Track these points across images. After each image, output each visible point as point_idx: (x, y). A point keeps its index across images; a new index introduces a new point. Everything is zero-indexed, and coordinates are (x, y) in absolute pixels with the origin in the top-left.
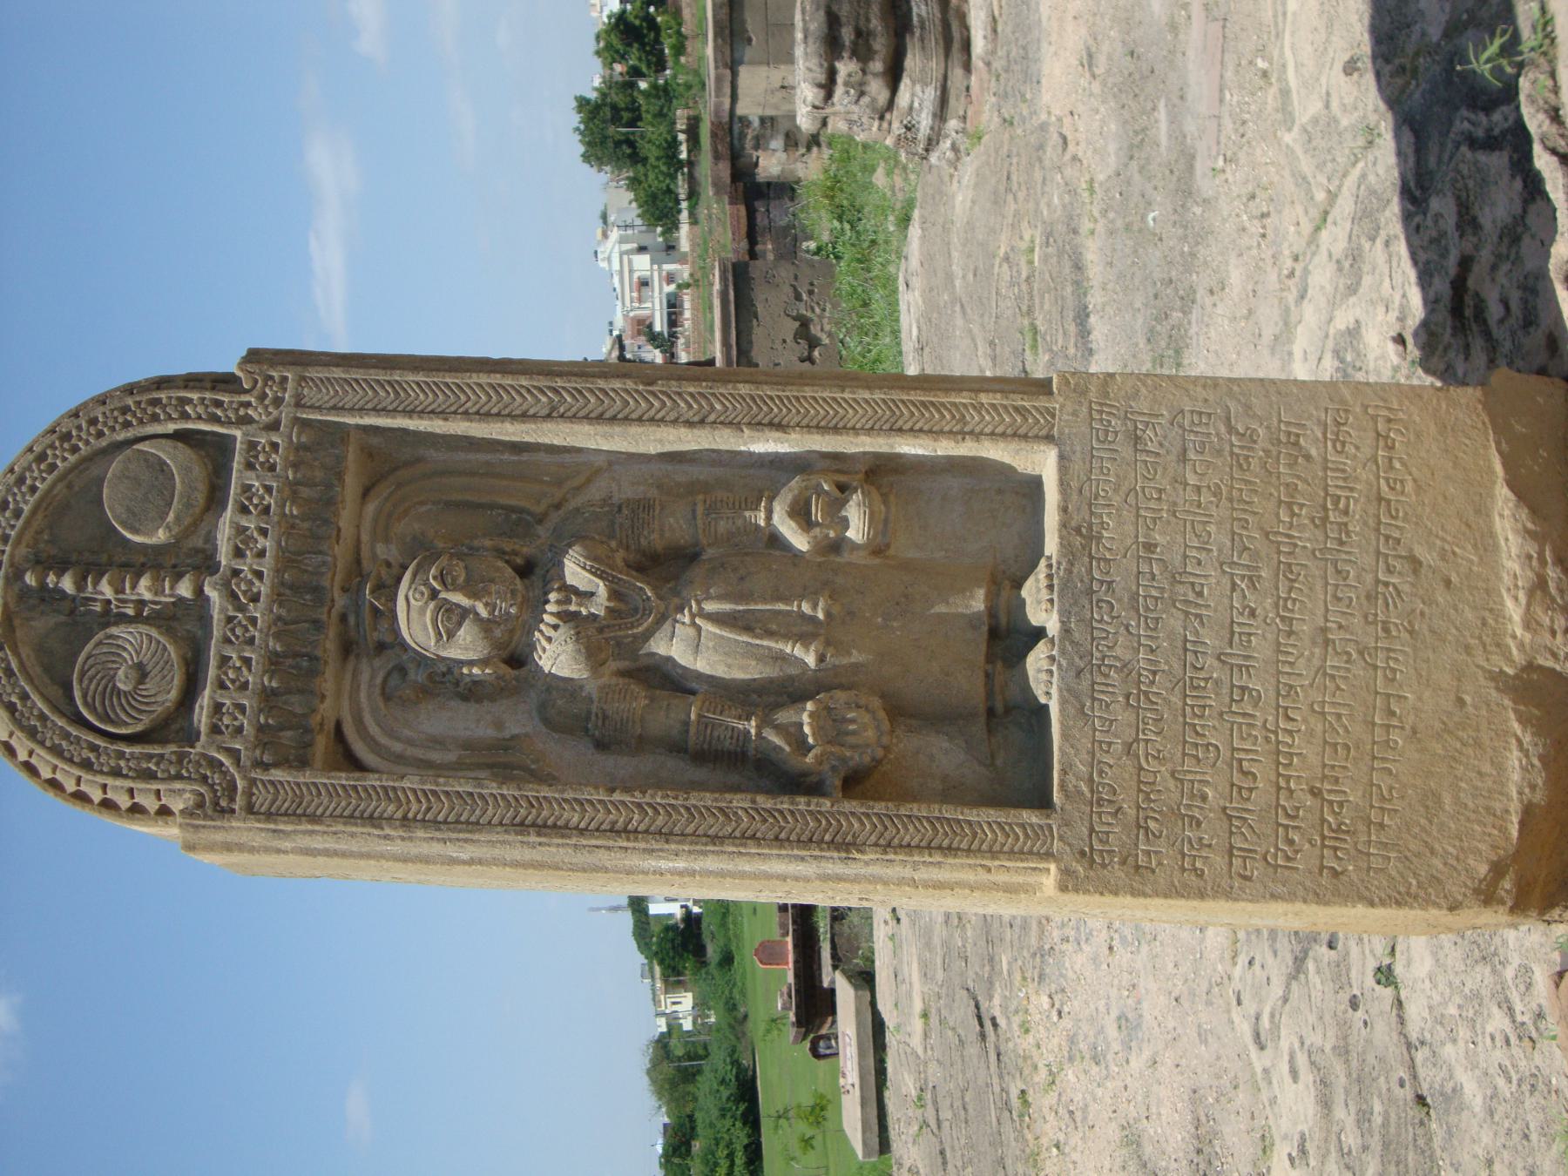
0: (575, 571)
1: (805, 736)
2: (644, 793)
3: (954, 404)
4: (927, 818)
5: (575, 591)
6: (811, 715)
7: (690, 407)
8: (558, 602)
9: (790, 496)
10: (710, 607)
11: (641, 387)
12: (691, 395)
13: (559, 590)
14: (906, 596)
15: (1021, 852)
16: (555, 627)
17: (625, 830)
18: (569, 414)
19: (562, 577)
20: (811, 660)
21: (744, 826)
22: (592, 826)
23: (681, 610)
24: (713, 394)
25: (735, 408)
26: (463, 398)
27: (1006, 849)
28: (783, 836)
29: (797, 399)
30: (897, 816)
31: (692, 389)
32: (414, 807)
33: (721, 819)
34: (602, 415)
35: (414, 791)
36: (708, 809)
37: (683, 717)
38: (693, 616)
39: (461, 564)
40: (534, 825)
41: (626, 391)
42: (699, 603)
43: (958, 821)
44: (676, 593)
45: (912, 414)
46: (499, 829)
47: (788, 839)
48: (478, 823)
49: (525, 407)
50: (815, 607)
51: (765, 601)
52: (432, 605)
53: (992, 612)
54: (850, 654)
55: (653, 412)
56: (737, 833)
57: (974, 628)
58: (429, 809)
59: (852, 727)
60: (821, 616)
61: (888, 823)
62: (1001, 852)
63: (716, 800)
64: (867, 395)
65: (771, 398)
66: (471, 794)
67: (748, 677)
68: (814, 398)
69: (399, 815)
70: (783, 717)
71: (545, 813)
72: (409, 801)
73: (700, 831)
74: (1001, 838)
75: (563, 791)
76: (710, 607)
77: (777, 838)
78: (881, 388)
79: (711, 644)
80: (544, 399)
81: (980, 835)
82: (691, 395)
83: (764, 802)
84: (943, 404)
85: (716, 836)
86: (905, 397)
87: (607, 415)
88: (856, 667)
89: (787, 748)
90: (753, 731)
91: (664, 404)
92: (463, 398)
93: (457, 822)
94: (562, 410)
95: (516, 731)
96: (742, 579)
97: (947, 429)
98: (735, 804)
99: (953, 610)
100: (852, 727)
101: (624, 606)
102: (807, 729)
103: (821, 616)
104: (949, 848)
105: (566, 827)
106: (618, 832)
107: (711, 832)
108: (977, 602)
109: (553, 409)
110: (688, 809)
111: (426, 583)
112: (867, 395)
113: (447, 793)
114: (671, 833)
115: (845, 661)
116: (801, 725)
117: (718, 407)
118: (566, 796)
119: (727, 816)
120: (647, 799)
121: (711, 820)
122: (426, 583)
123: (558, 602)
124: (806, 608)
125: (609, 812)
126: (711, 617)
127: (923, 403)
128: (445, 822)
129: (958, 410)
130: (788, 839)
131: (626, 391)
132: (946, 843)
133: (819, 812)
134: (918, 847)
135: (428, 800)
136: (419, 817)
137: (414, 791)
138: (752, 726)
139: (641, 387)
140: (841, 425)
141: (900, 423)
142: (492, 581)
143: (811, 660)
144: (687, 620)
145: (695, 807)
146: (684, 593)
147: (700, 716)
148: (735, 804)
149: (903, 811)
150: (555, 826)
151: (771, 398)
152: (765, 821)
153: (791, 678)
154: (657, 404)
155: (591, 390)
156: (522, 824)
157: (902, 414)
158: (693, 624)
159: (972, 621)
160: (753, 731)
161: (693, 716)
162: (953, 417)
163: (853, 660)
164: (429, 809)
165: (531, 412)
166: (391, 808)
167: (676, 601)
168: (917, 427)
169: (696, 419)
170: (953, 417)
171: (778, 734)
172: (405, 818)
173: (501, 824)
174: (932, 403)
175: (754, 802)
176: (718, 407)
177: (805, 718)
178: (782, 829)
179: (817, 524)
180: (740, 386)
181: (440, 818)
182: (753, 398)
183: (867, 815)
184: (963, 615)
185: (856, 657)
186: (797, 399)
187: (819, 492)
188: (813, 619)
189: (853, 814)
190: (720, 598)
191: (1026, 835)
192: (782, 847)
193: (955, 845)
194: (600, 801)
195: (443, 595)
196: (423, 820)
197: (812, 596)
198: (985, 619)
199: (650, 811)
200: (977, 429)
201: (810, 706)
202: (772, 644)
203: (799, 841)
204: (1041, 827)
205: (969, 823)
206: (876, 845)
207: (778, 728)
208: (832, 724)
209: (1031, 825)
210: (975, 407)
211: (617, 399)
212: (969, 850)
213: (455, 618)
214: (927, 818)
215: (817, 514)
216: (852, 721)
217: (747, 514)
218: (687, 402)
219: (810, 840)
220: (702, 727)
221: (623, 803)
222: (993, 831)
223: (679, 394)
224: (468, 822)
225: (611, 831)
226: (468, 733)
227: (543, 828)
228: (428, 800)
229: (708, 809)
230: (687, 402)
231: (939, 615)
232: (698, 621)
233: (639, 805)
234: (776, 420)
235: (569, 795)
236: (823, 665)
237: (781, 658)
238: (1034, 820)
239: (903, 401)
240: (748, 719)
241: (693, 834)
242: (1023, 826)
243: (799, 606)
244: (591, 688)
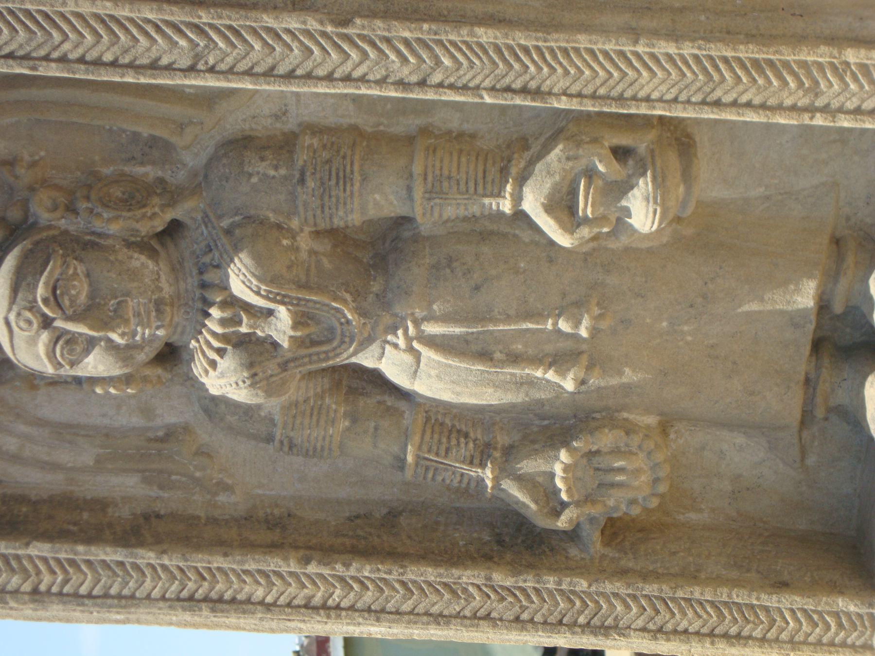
0: (241, 280)
1: (556, 491)
2: (347, 565)
3: (804, 64)
4: (712, 603)
5: (247, 307)
6: (566, 469)
7: (405, 60)
8: (223, 322)
9: (548, 185)
10: (432, 329)
11: (329, 29)
12: (406, 42)
13: (224, 305)
14: (705, 297)
15: (832, 644)
16: (221, 352)
17: (324, 607)
18: (223, 67)
19: (226, 288)
20: (569, 385)
21: (475, 604)
22: (282, 600)
23: (394, 330)
24: (440, 43)
25: (472, 64)
26: (57, 36)
27: (811, 639)
28: (525, 616)
29: (565, 51)
30: (673, 599)
31: (407, 34)
32: (47, 579)
33: (447, 596)
34: (273, 68)
35: (45, 560)
36: (430, 584)
37: (396, 449)
38: (409, 339)
39: (81, 269)
40: (206, 599)
41: (308, 33)
42: (417, 323)
43: (752, 607)
44: (384, 302)
45: (738, 79)
46: (161, 604)
47: (531, 620)
48: (132, 597)
49: (154, 54)
50: (577, 324)
51: (508, 319)
52: (45, 336)
53: (823, 306)
54: (620, 373)
55: (349, 65)
56: (467, 613)
57: (796, 326)
58: (66, 581)
59: (620, 478)
60: (584, 333)
61: (660, 606)
62: (805, 643)
63: (440, 575)
64: (672, 49)
65: (526, 50)
66: (121, 564)
67: (484, 403)
68: (592, 52)
69: (27, 587)
70: (529, 466)
71: (220, 587)
72: (38, 573)
73: (420, 609)
74: (806, 627)
75: (242, 562)
76: (432, 329)
77: (517, 619)
78: (693, 40)
79: (433, 373)
80: (183, 43)
81: (779, 622)
82: (406, 42)
83: (501, 578)
84: (786, 65)
85: (441, 615)
86: (729, 54)
87: (281, 70)
88: (627, 389)
89: (533, 506)
90: (489, 484)
91: (365, 54)
92: (57, 36)
93: (106, 596)
94: (211, 61)
95: (171, 419)
96: (477, 288)
97: (788, 102)
98: (465, 579)
99: (769, 307)
100: (620, 478)
101: (315, 333)
102: (559, 484)
103: (584, 333)
104: (738, 636)
105: (248, 601)
106: (315, 609)
107: (435, 610)
108: (805, 297)
109: (197, 57)
110: (403, 584)
111: (32, 307)
112: (672, 49)
113: (89, 563)
114: (383, 611)
115: (614, 381)
116: (552, 475)
117: (447, 61)
118: (246, 567)
119: (454, 592)
120: (352, 572)
121: (433, 598)
122: (32, 307)
123: (223, 322)
124: (564, 326)
125: (304, 586)
126: (432, 342)
127: (756, 63)
128: (90, 596)
129: (809, 74)
130: (531, 620)
131: (308, 33)
132: (733, 630)
133: (573, 592)
134: (697, 633)
135: (65, 571)
136: (55, 589)
137: (45, 560)
138: (488, 475)
139: (329, 29)
140: (628, 94)
141: (718, 93)
142: (128, 294)
143: (569, 385)
144: (401, 342)
145: (414, 582)
146: (398, 309)
147: (418, 457)
148: (465, 579)
149: (680, 594)
150: (233, 600)
151: (526, 50)
152: (503, 599)
153: (541, 403)
154: (354, 55)
155: (254, 32)
156: (191, 598)
157: (723, 80)
158: (411, 349)
159: (794, 319)
160: (489, 484)
161: (410, 458)
162: (801, 84)
163: (624, 380)
164: (66, 581)
165: (165, 61)
166: (15, 580)
167: (387, 320)
168: (744, 99)
169: (414, 79)
170: (801, 84)
171: (520, 489)
172: (35, 591)
173: (163, 598)
174: (771, 63)
175: (489, 579)
176: (447, 61)
177: (558, 469)
178: (523, 609)
179: (586, 220)
180: (480, 31)
181: (83, 590)
182: (498, 49)
183: (634, 597)
184: (782, 312)
185: (629, 376)
186: (565, 51)
187: (590, 174)
188: (575, 337)
189: (616, 595)
190: (446, 319)
191: (840, 626)
192: (523, 629)
193: (745, 633)
194: (291, 574)
195: (59, 323)
196: (60, 594)
197: (573, 307)
198: (813, 317)
199: (356, 586)
200: (835, 104)
201: (564, 455)
202: (517, 371)
203: (545, 623)
204: (860, 616)
205: (766, 609)
206: (644, 629)
207: (521, 480)
208: (595, 475)
209: (848, 615)
210: (834, 68)
211: (295, 45)
212: (763, 640)
213: (79, 349)
214: (712, 603)
215: (585, 207)
216: (621, 470)
217: (487, 201)
218: (399, 53)
219: (560, 623)
220: (420, 471)
221: (322, 576)
222: (797, 620)
223: (388, 40)
224: (119, 597)
225: (306, 606)
226: (106, 421)
227: (218, 604)
228: (65, 571)
229: (430, 584)
230: (399, 53)
231: (748, 314)
232: (415, 345)
233: (342, 579)
234: (533, 85)
235: (251, 566)
236: (583, 388)
237: (531, 382)
238: (852, 608)
239: (725, 60)
240: (482, 465)
241: (411, 613)
242: (837, 615)
243: (555, 324)
244: (273, 405)
